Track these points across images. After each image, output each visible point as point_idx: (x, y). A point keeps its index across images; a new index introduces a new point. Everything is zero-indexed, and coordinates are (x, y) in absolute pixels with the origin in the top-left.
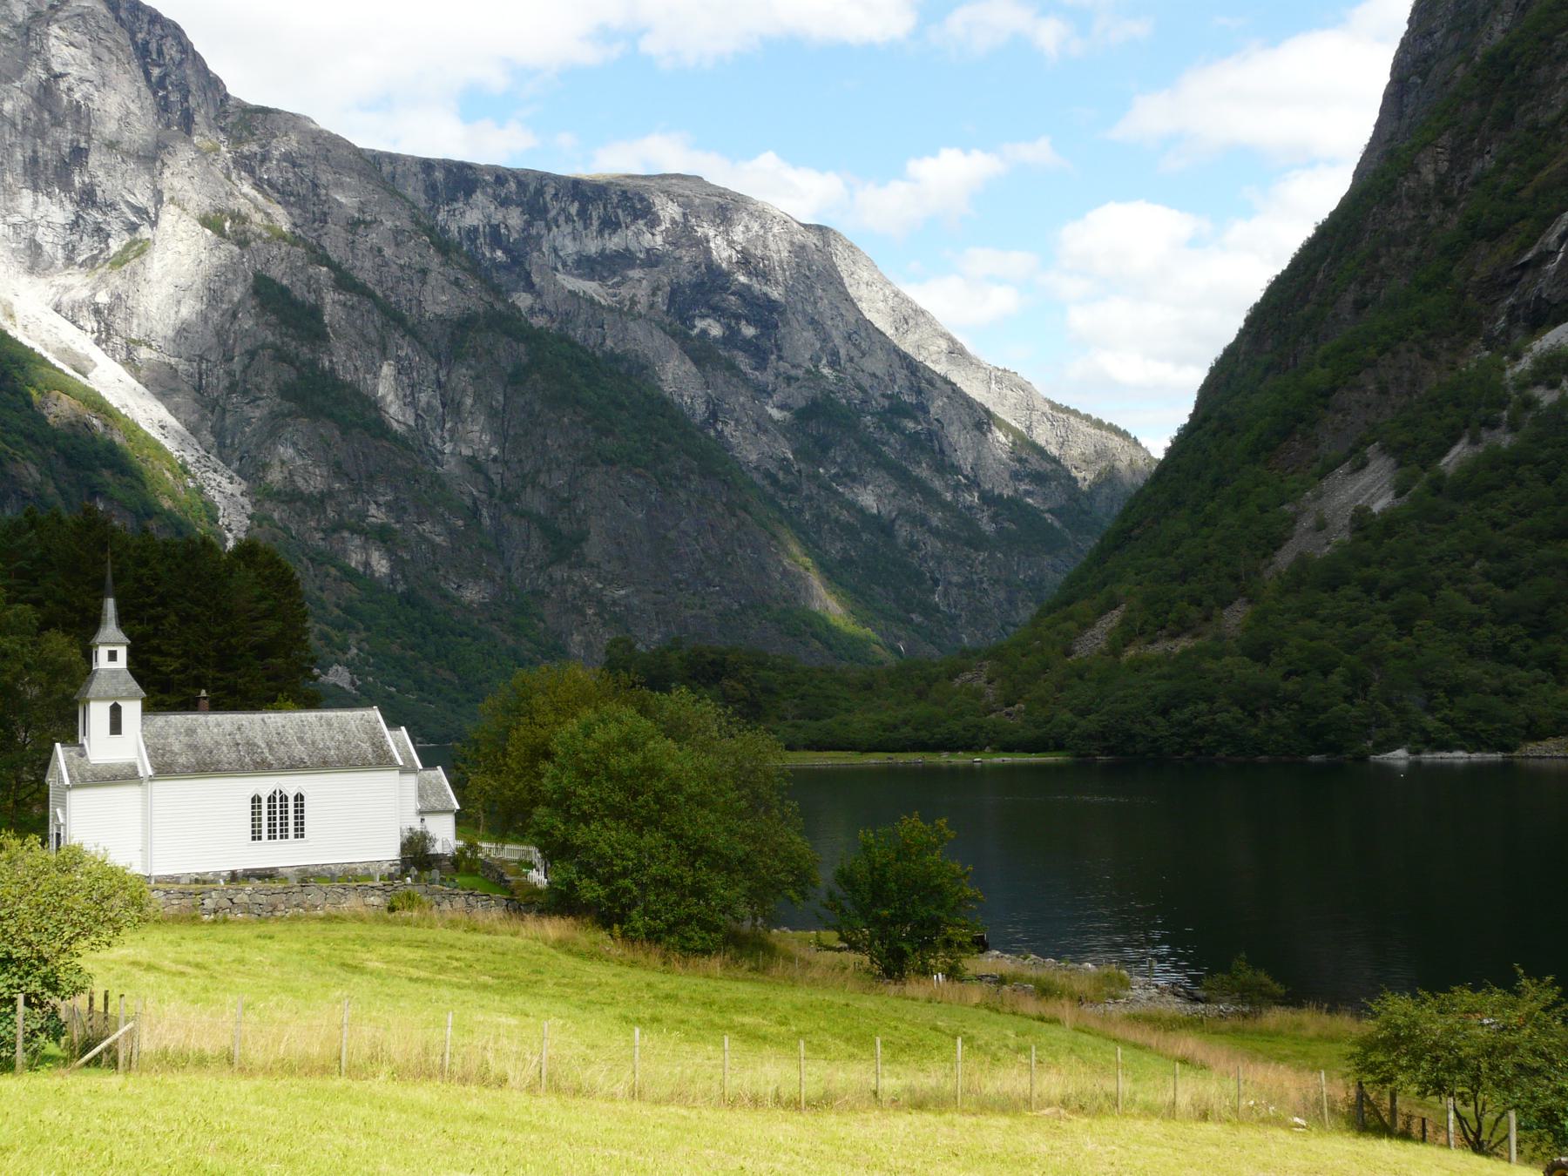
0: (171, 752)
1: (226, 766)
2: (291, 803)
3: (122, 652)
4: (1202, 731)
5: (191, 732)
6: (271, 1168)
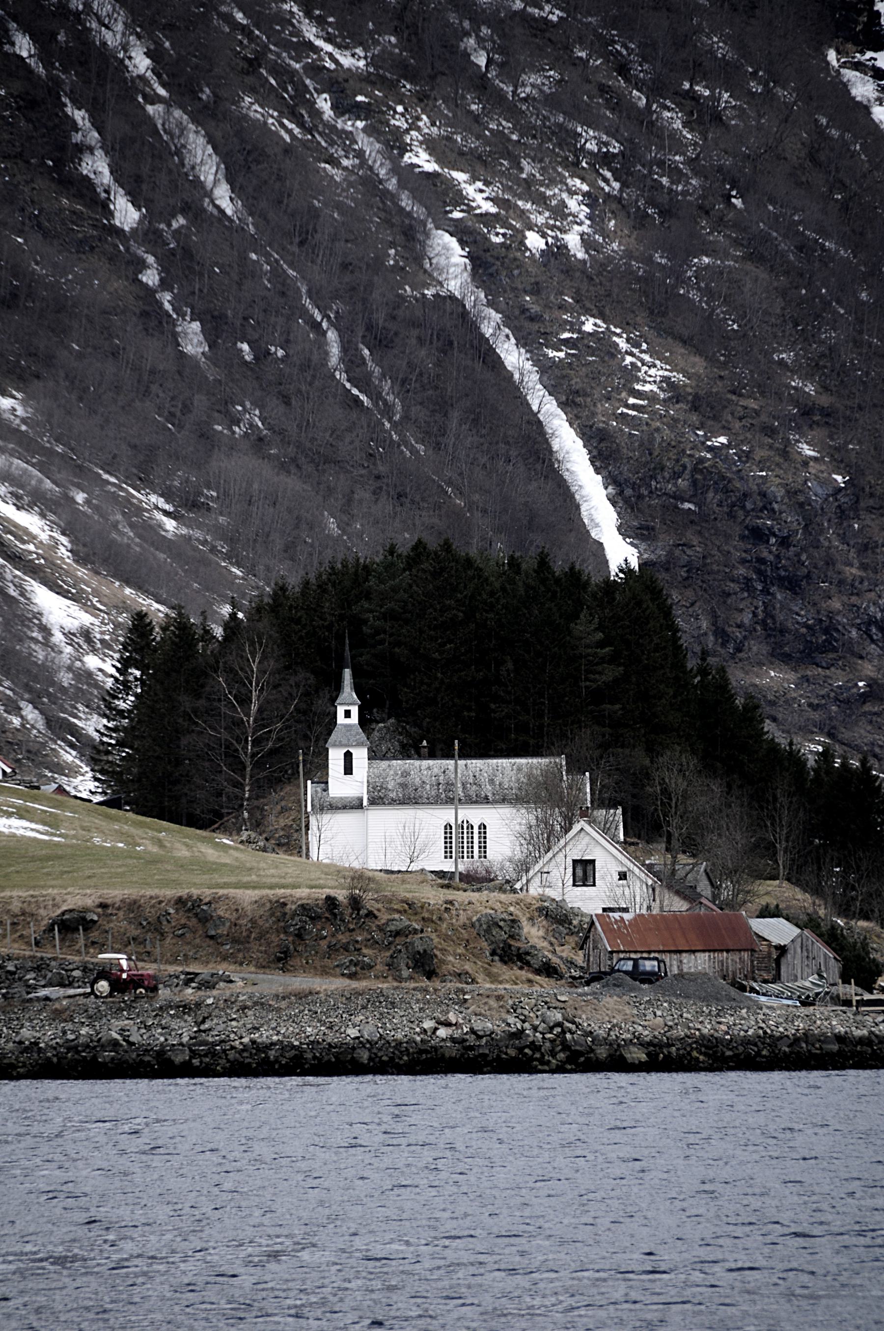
0: (386, 789)
1: (425, 800)
2: (476, 830)
3: (355, 711)
4: (837, 630)
5: (405, 774)
6: (199, 1325)
